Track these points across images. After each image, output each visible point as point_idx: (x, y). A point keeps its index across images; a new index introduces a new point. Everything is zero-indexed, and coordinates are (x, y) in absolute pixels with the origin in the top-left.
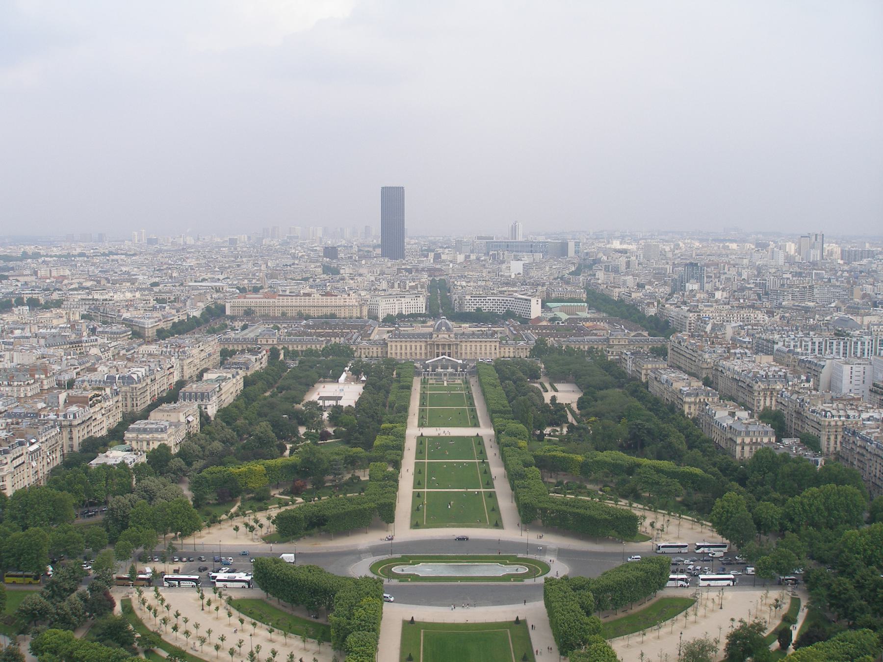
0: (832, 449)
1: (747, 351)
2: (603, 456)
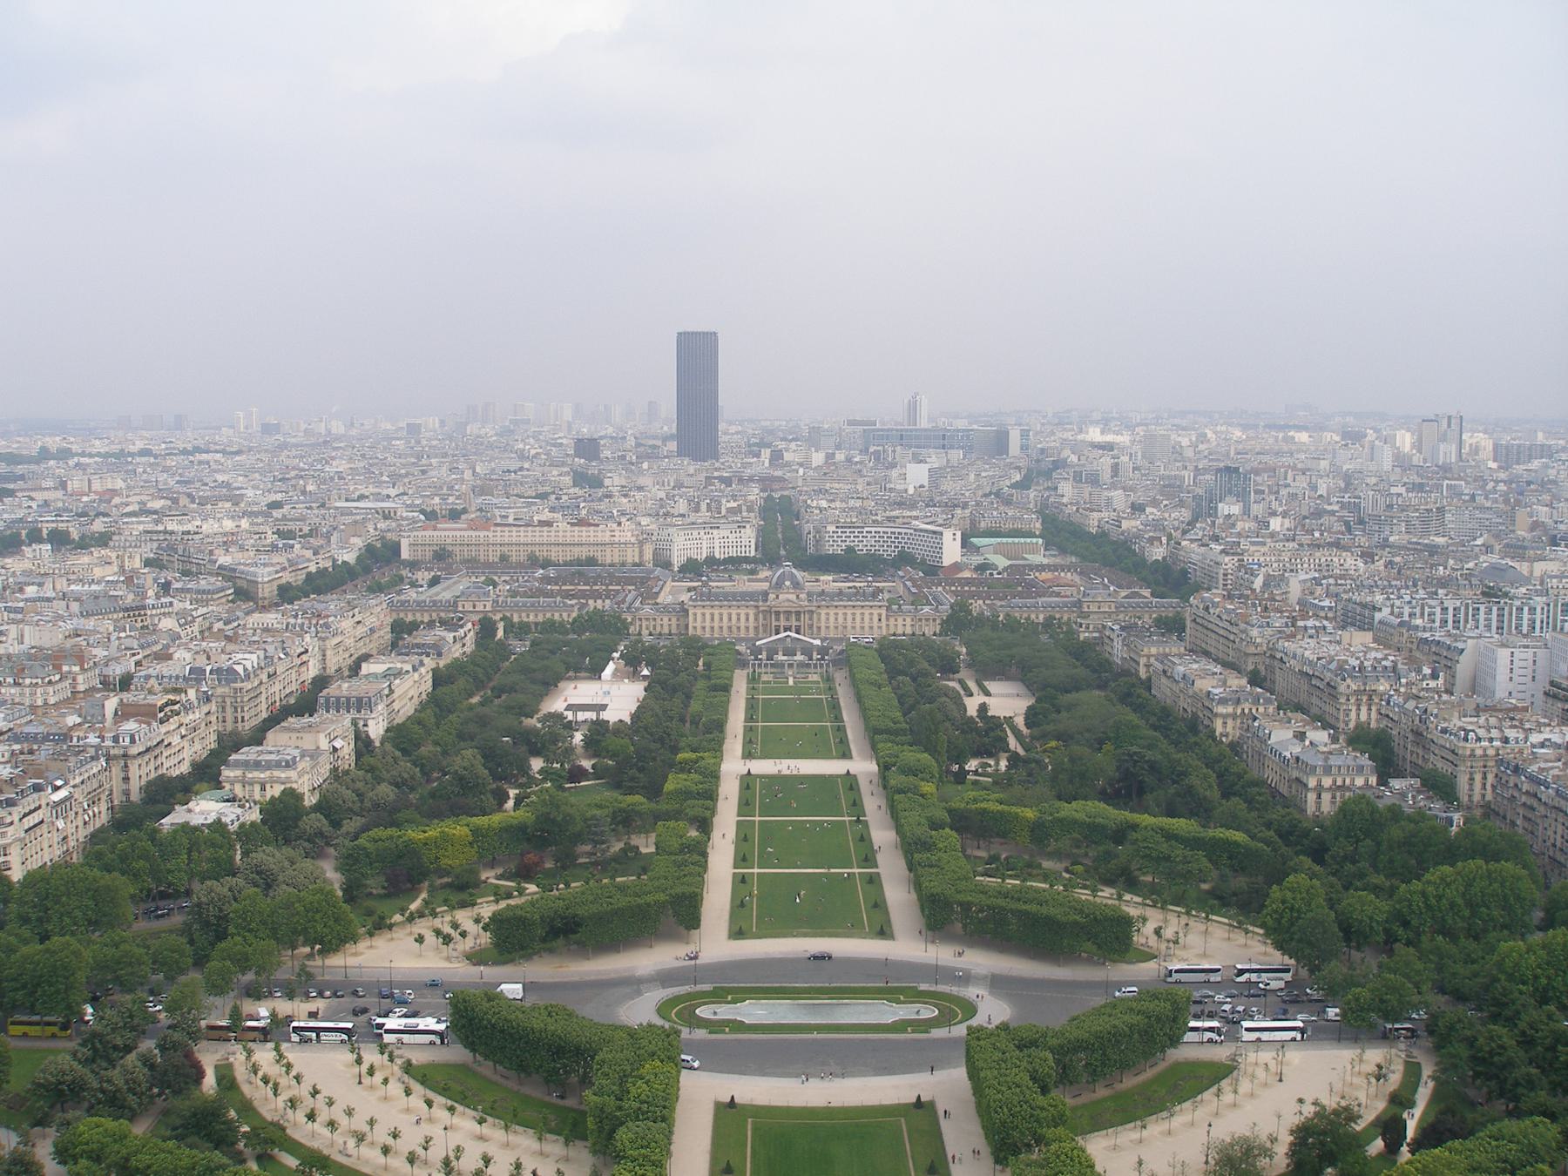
0: (1477, 798)
1: (1326, 623)
2: (1070, 810)
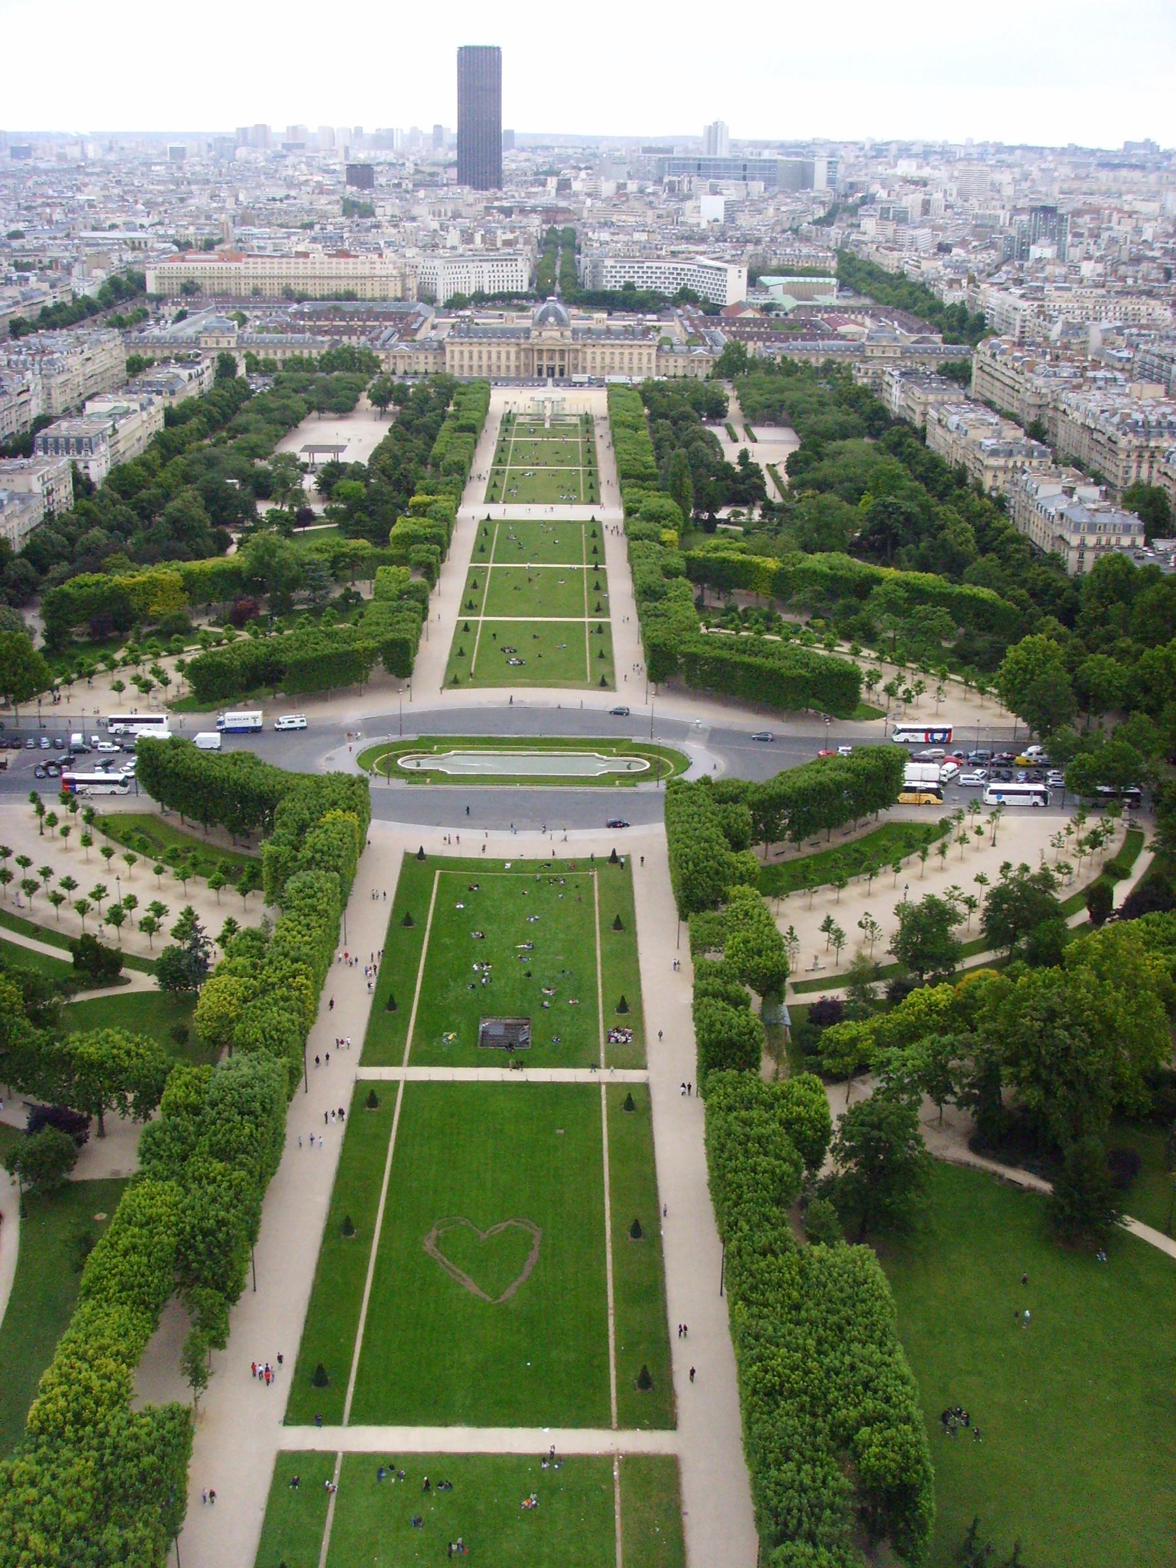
1: (1118, 375)
2: (816, 561)
